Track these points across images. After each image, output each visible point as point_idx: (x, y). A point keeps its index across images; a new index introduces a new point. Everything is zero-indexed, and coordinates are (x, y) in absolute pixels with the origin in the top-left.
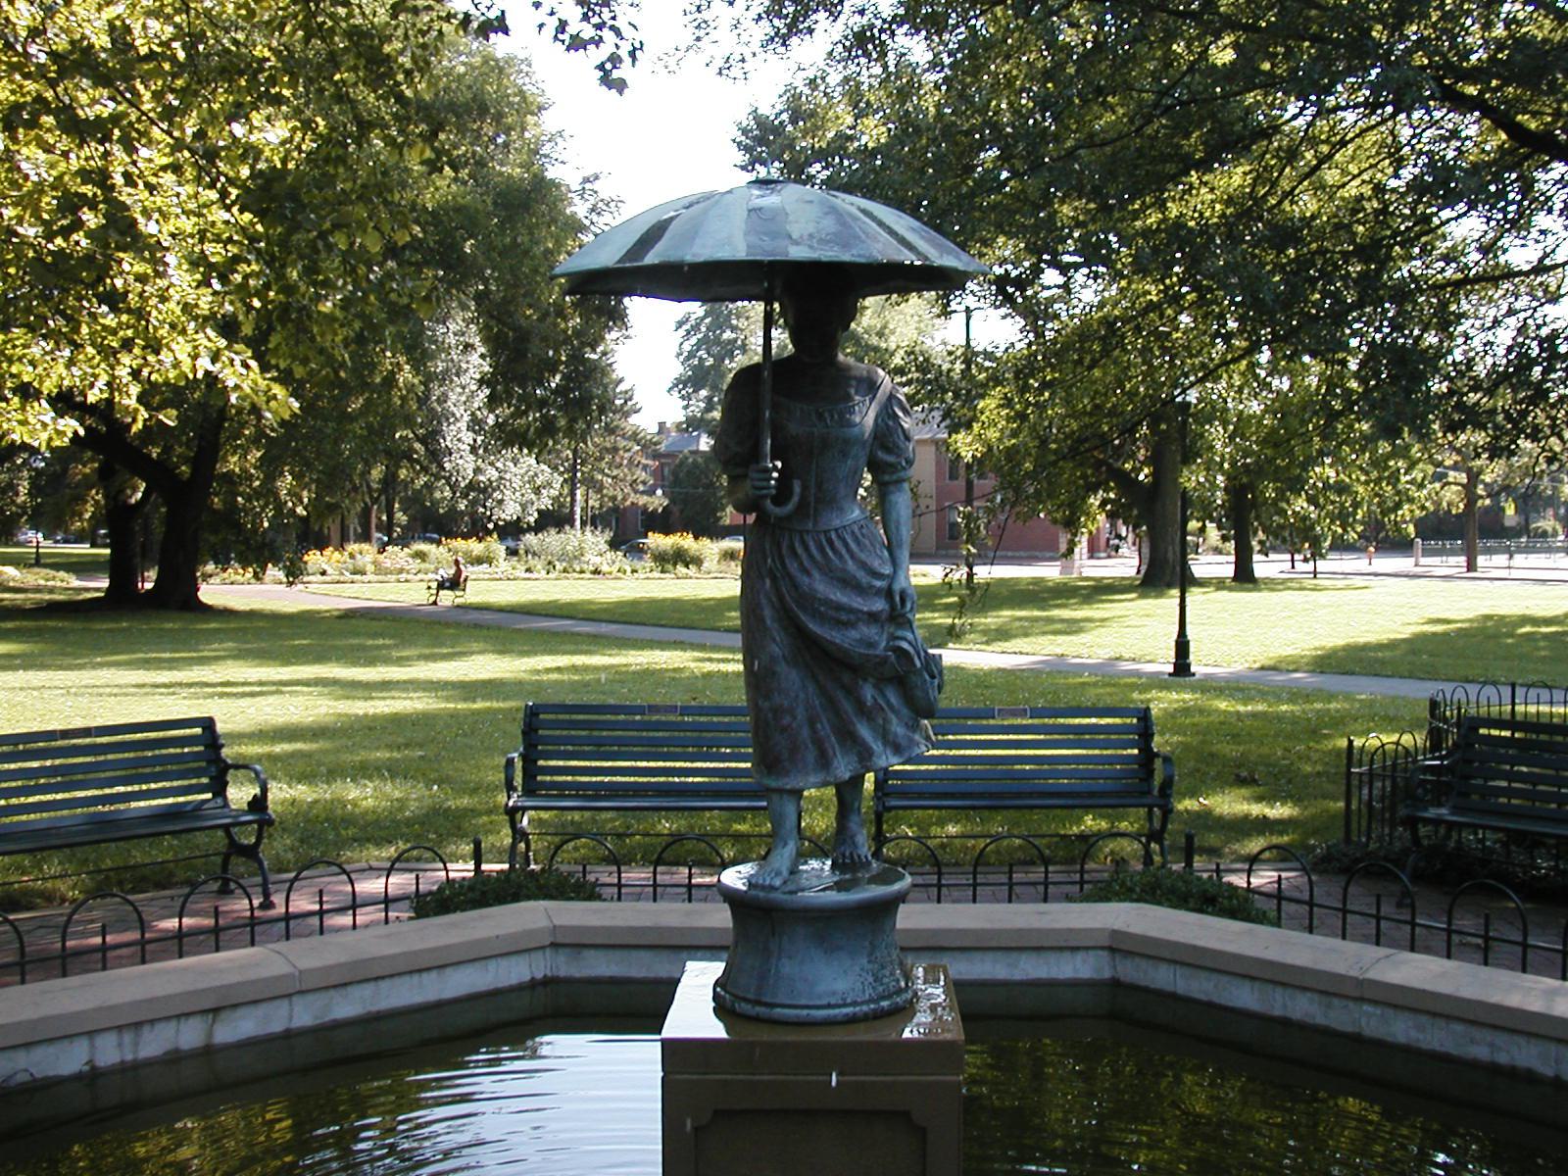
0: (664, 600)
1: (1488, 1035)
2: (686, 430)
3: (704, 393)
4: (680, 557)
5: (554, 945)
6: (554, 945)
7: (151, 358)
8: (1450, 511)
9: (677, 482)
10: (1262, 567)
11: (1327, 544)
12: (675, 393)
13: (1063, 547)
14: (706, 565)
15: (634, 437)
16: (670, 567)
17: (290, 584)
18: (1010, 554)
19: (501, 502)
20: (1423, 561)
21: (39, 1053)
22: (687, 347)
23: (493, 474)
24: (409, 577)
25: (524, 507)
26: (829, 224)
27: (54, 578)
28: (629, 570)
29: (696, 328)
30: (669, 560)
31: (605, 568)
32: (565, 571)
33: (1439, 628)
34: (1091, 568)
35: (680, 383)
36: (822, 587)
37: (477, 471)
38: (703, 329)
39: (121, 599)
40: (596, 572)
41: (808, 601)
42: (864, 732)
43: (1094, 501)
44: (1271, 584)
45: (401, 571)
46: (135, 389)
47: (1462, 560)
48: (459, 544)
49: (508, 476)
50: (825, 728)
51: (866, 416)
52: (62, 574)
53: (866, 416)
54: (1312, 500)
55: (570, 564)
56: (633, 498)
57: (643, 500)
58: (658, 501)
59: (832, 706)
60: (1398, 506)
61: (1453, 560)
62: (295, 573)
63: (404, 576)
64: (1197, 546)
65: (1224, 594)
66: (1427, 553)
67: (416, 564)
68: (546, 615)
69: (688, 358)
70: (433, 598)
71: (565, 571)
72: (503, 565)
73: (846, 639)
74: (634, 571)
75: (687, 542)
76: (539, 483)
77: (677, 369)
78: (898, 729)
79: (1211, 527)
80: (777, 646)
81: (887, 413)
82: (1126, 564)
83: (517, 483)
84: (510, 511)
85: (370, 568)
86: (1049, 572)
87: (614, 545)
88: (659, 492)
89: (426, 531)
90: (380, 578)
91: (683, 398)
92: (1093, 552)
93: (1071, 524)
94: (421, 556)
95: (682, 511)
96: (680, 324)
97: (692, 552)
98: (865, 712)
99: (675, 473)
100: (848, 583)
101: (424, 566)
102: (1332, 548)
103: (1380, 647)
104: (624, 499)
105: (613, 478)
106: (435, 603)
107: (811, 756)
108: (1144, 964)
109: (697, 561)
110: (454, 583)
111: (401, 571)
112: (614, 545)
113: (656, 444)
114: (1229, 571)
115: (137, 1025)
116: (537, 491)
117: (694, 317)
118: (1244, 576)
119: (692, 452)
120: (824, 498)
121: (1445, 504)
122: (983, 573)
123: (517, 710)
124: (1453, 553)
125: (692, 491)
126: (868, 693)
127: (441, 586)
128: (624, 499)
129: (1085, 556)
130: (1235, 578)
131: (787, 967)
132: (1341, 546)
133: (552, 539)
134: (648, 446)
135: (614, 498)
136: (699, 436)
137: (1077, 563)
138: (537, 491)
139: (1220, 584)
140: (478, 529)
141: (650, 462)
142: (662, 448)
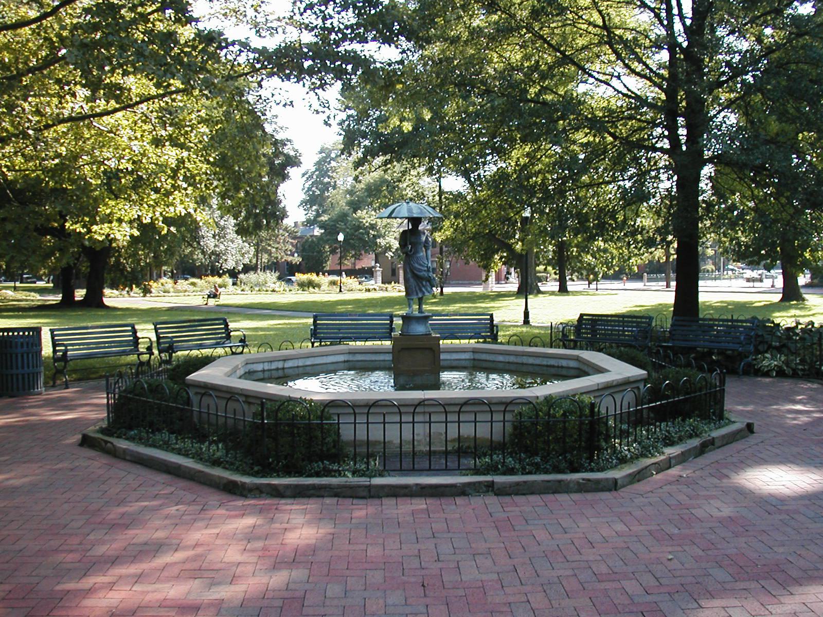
0: (308, 302)
1: (545, 359)
2: (306, 225)
3: (314, 208)
4: (311, 284)
5: (349, 353)
6: (349, 353)
7: (167, 209)
8: (659, 261)
9: (304, 250)
10: (571, 286)
11: (600, 276)
12: (301, 207)
13: (484, 278)
14: (322, 288)
15: (286, 229)
16: (306, 288)
17: (144, 296)
18: (460, 282)
19: (226, 260)
20: (648, 284)
21: (255, 365)
22: (307, 186)
23: (222, 247)
24: (190, 294)
25: (237, 263)
26: (419, 211)
27: (29, 296)
28: (288, 290)
29: (311, 177)
30: (303, 285)
31: (277, 289)
32: (259, 290)
33: (638, 309)
34: (494, 287)
35: (304, 203)
36: (416, 265)
37: (216, 246)
38: (315, 177)
39: (68, 303)
40: (273, 291)
41: (415, 268)
42: (424, 289)
43: (497, 257)
44: (575, 293)
45: (185, 291)
46: (161, 219)
47: (665, 283)
48: (210, 278)
49: (229, 248)
50: (417, 289)
51: (424, 238)
52: (33, 294)
53: (424, 238)
54: (594, 256)
55: (260, 287)
56: (285, 258)
57: (290, 259)
58: (296, 259)
59: (418, 285)
60: (630, 258)
61: (661, 283)
62: (146, 291)
63: (187, 293)
64: (547, 278)
65: (553, 297)
66: (649, 280)
67: (192, 288)
68: (258, 309)
69: (308, 191)
70: (205, 302)
71: (259, 290)
72: (231, 288)
73: (421, 274)
74: (290, 290)
75: (313, 277)
76: (243, 251)
77: (303, 196)
78: (429, 289)
79: (550, 268)
80: (409, 275)
81: (427, 238)
82: (513, 285)
83: (234, 252)
84: (230, 265)
85: (172, 290)
86: (478, 289)
87: (279, 278)
88: (296, 255)
89: (184, 274)
90: (177, 294)
91: (305, 210)
92: (498, 280)
93: (487, 268)
94: (194, 284)
95: (306, 264)
96: (304, 175)
97: (316, 282)
98: (424, 286)
99: (303, 246)
100: (421, 265)
101: (195, 289)
102: (603, 277)
103: (612, 316)
104: (282, 258)
105: (277, 248)
106: (206, 304)
107: (415, 293)
108: (480, 354)
109: (319, 286)
110: (214, 296)
111: (185, 291)
112: (279, 278)
113: (296, 232)
114: (557, 288)
115: (271, 362)
116: (243, 255)
117: (310, 172)
118: (563, 290)
119: (311, 236)
120: (416, 252)
121: (656, 258)
122: (447, 290)
123: (103, 419)
124: (661, 280)
125: (311, 254)
126: (424, 283)
127: (209, 297)
128: (282, 258)
129: (494, 282)
130: (559, 291)
131: (412, 327)
132: (606, 277)
133: (252, 276)
134: (293, 235)
135: (277, 258)
136: (314, 228)
137: (490, 286)
138: (243, 255)
139: (552, 293)
140: (216, 272)
141: (293, 241)
142: (299, 234)
